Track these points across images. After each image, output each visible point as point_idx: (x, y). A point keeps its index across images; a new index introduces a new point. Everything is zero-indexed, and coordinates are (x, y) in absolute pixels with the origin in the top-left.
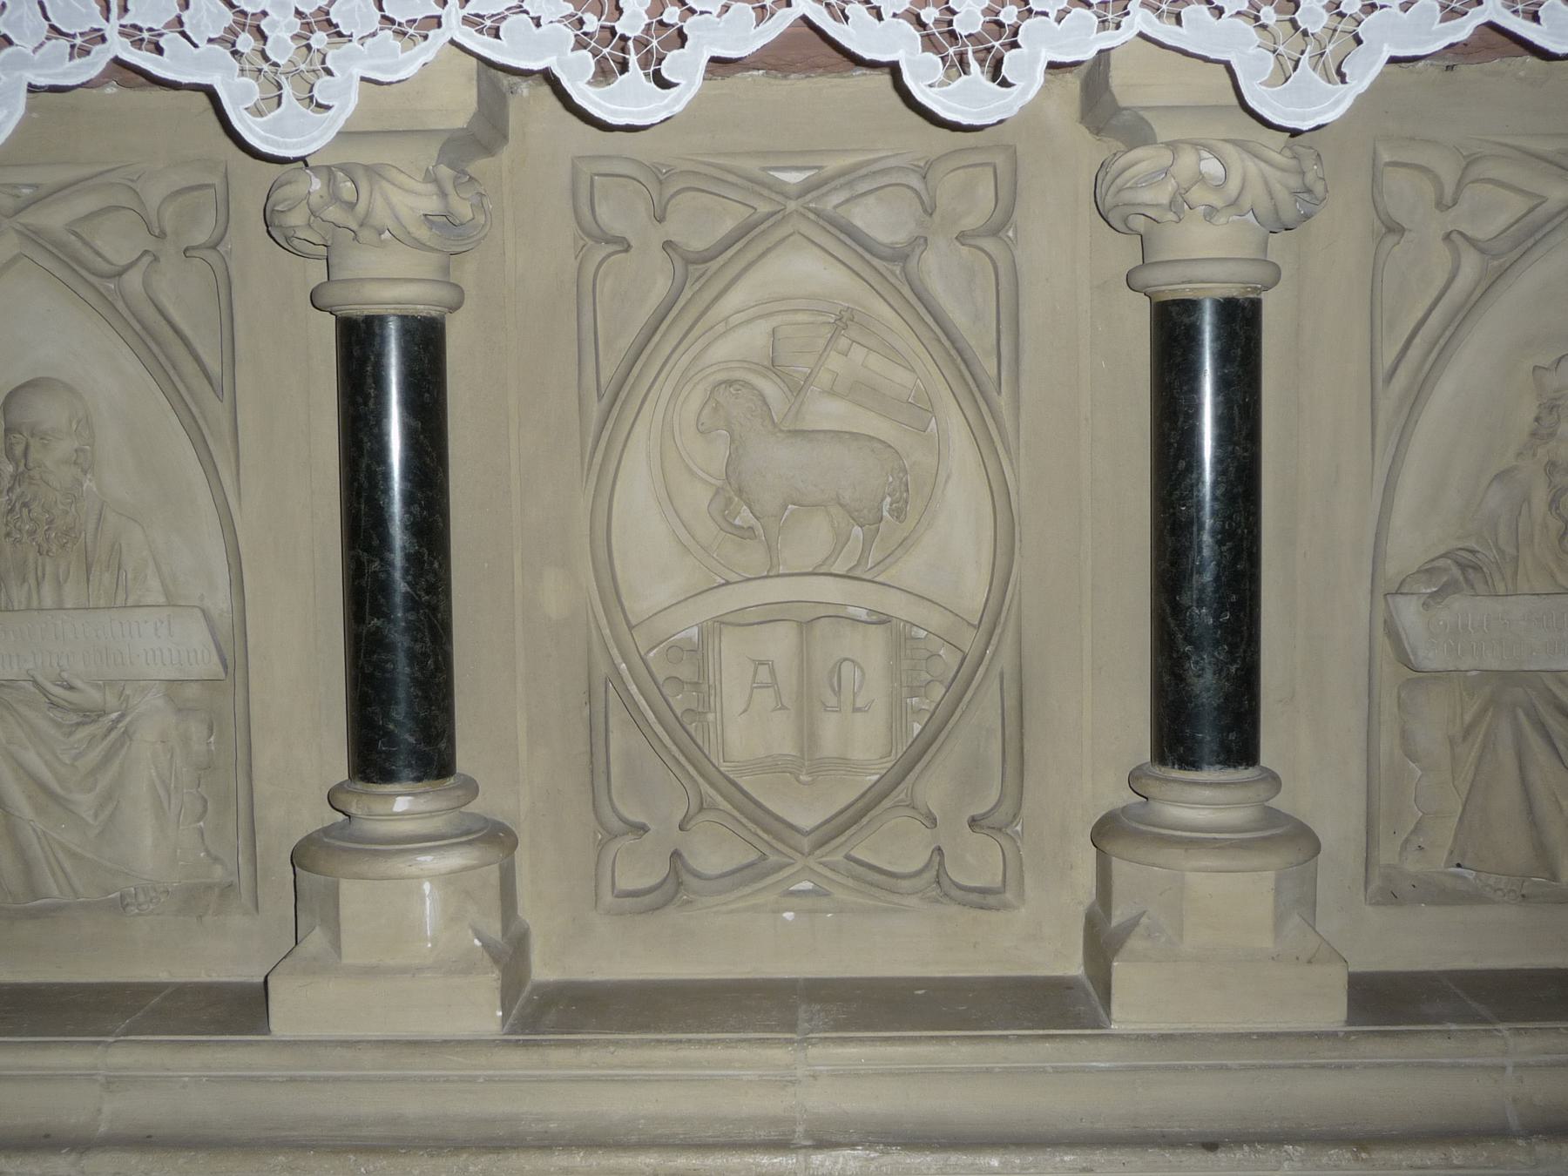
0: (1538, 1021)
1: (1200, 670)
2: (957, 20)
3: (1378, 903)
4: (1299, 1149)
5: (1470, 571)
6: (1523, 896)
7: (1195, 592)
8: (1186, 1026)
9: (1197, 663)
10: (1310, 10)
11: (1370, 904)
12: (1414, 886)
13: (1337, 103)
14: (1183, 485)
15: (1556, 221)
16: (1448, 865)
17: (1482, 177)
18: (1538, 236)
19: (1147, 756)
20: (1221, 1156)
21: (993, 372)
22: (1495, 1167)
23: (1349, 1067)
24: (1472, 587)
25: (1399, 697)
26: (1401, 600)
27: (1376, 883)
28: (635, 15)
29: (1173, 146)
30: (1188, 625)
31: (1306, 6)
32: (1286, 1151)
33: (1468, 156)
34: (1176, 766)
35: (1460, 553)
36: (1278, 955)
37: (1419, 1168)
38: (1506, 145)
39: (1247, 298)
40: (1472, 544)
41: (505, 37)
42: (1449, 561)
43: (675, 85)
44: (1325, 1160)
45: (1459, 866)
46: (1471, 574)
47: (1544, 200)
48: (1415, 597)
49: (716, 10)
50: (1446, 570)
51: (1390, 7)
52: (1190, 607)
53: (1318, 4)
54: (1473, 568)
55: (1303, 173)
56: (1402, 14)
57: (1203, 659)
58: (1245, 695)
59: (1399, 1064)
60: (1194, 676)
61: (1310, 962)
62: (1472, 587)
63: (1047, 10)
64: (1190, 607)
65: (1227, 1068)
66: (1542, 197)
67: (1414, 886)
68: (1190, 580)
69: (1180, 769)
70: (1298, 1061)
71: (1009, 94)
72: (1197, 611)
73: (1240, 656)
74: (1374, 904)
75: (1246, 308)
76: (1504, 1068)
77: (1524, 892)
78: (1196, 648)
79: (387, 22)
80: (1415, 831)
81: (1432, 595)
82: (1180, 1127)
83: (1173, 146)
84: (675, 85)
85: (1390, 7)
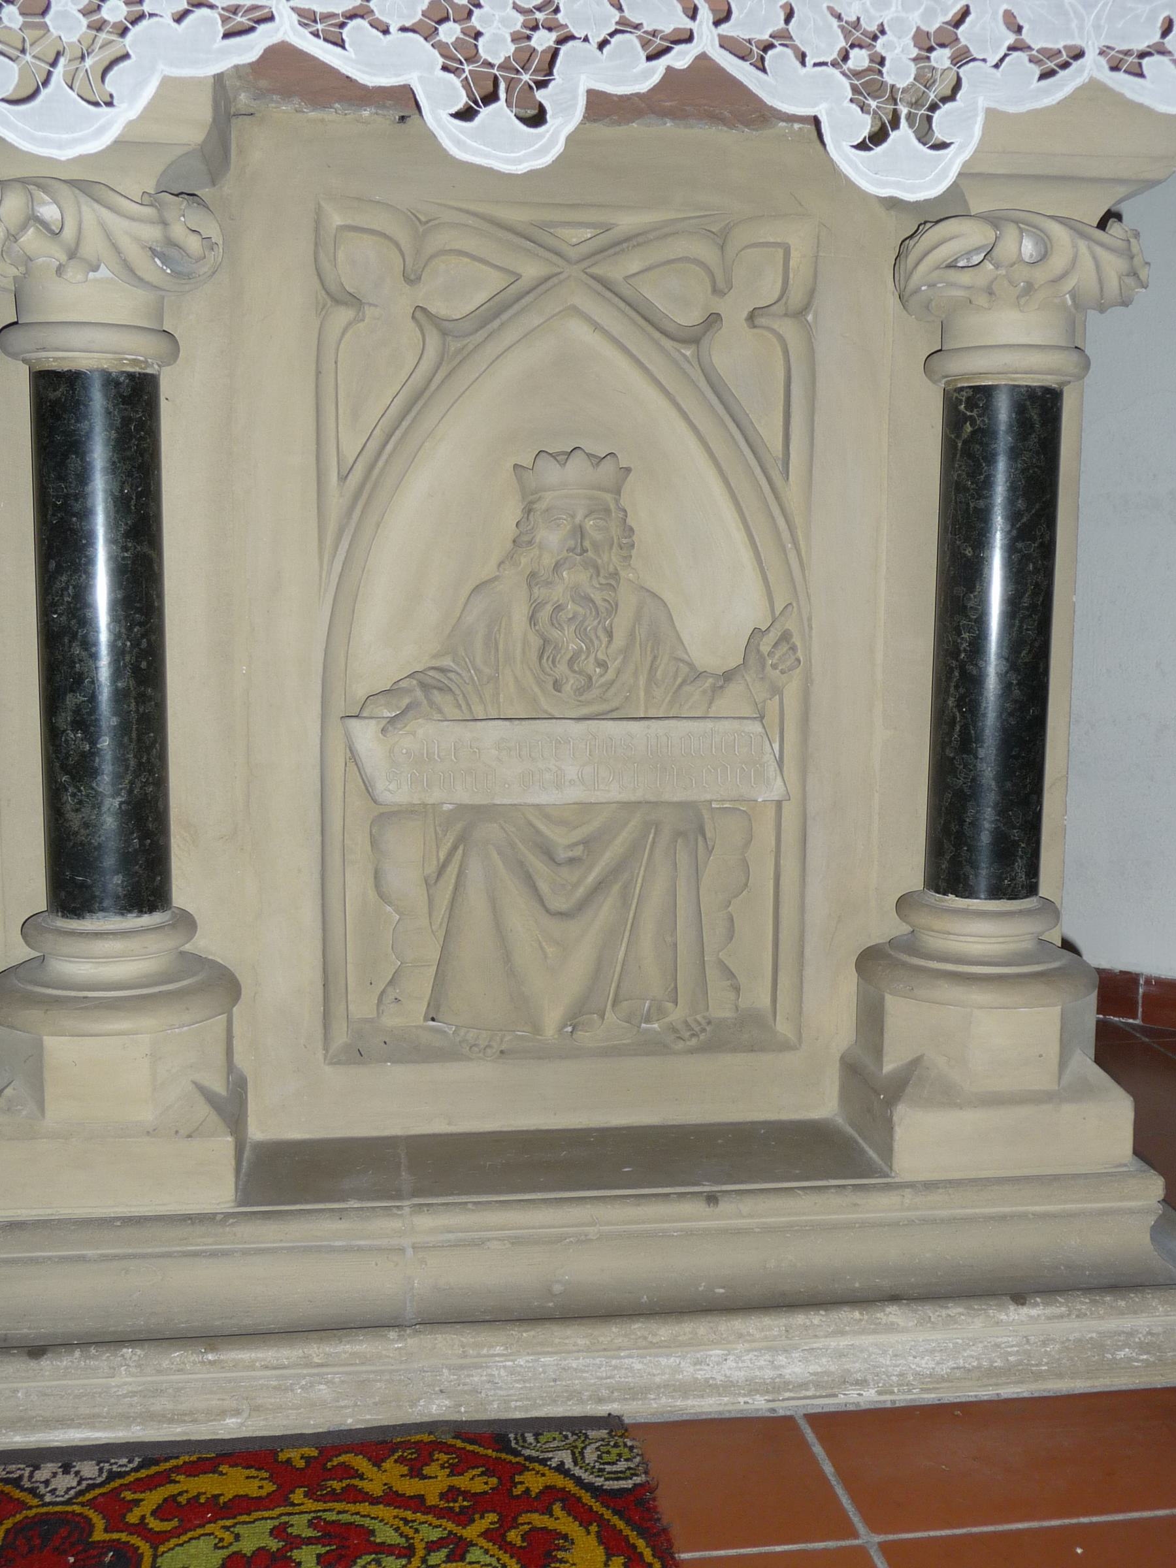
0: (456, 1194)
1: (77, 803)
2: (50, 20)
3: (339, 1063)
4: (139, 1352)
5: (436, 692)
6: (502, 1052)
7: (70, 713)
8: (49, 1211)
9: (74, 795)
10: (64, 14)
11: (331, 1064)
12: (385, 1043)
13: (101, 131)
14: (54, 589)
15: (524, 302)
16: (425, 1019)
17: (448, 248)
18: (505, 317)
19: (41, 904)
20: (46, 1364)
21: (777, 445)
22: (363, 1364)
23: (225, 1254)
24: (440, 711)
25: (371, 831)
26: (354, 724)
27: (341, 1037)
28: (497, 39)
29: (994, 220)
30: (64, 751)
31: (60, 8)
32: (123, 1356)
33: (427, 222)
34: (60, 914)
35: (432, 673)
36: (154, 1130)
37: (275, 1368)
38: (467, 212)
39: (124, 372)
40: (447, 662)
41: (351, 45)
42: (415, 682)
43: (952, 143)
44: (165, 1364)
45: (433, 1019)
46: (437, 696)
47: (518, 277)
48: (373, 722)
49: (595, 40)
50: (408, 691)
51: (161, 16)
52: (64, 731)
53: (73, 7)
54: (440, 689)
55: (165, 223)
56: (175, 25)
57: (80, 791)
58: (133, 833)
59: (282, 1248)
60: (73, 811)
61: (189, 1136)
62: (440, 711)
63: (299, 27)
64: (64, 731)
65: (83, 1259)
66: (518, 274)
67: (385, 1043)
68: (64, 700)
69: (63, 916)
70: (167, 1249)
71: (541, 136)
72: (72, 736)
73: (124, 788)
74: (335, 1064)
75: (121, 383)
76: (402, 1250)
77: (503, 1047)
78: (73, 778)
79: (655, 52)
80: (391, 983)
81: (392, 720)
82: (29, 1328)
83: (994, 220)
84: (952, 143)
85: (161, 16)
